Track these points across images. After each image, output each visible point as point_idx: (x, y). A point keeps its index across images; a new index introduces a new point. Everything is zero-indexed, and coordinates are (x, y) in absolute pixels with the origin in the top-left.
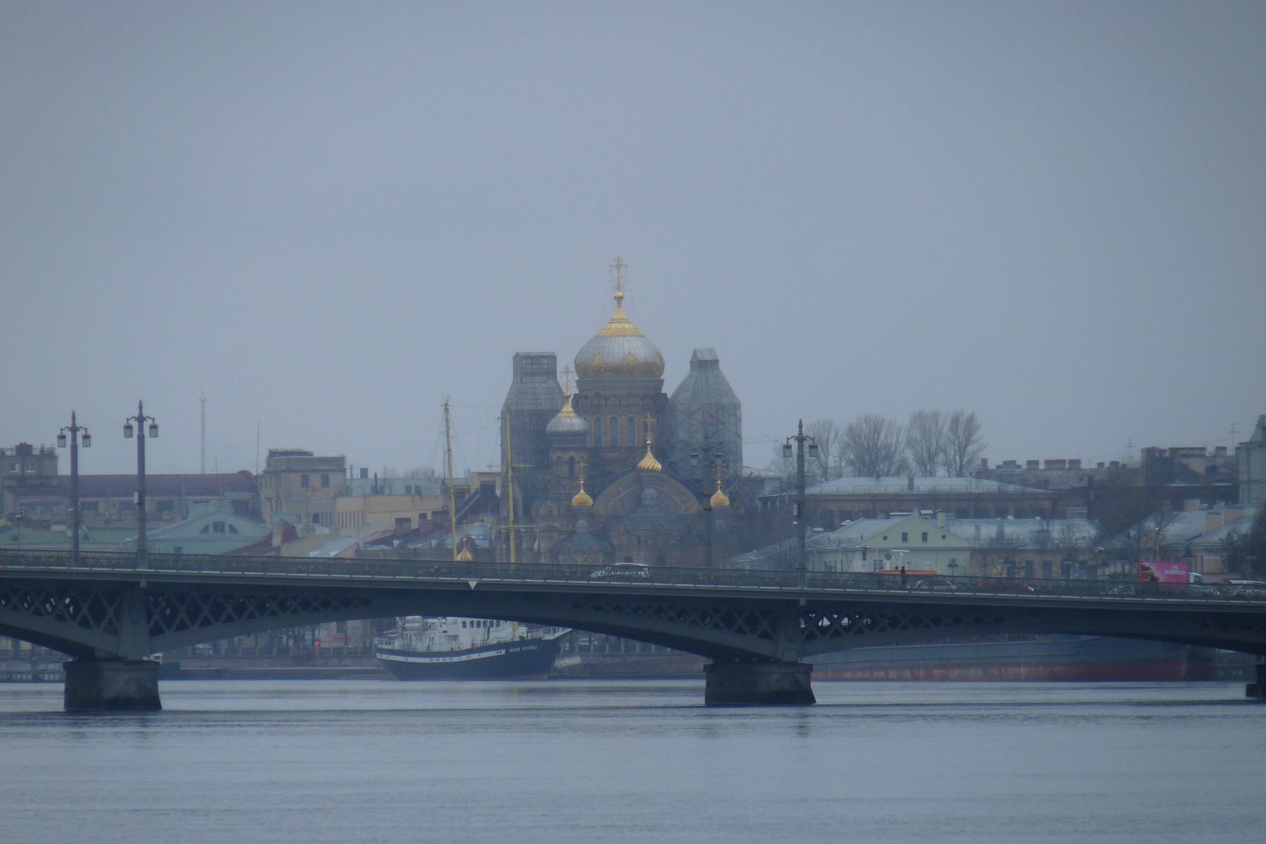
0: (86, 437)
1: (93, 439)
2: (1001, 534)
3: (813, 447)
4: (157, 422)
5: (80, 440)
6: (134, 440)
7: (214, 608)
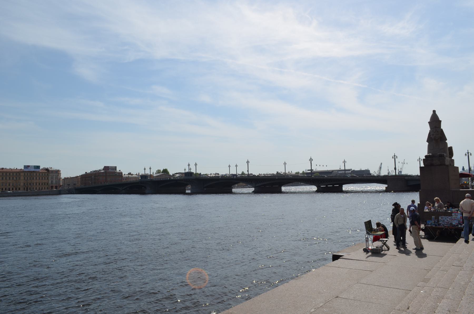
0: (346, 162)
1: (472, 154)
2: (129, 176)
3: (397, 157)
4: (471, 153)
5: (469, 155)
6: (467, 156)
7: (188, 180)
